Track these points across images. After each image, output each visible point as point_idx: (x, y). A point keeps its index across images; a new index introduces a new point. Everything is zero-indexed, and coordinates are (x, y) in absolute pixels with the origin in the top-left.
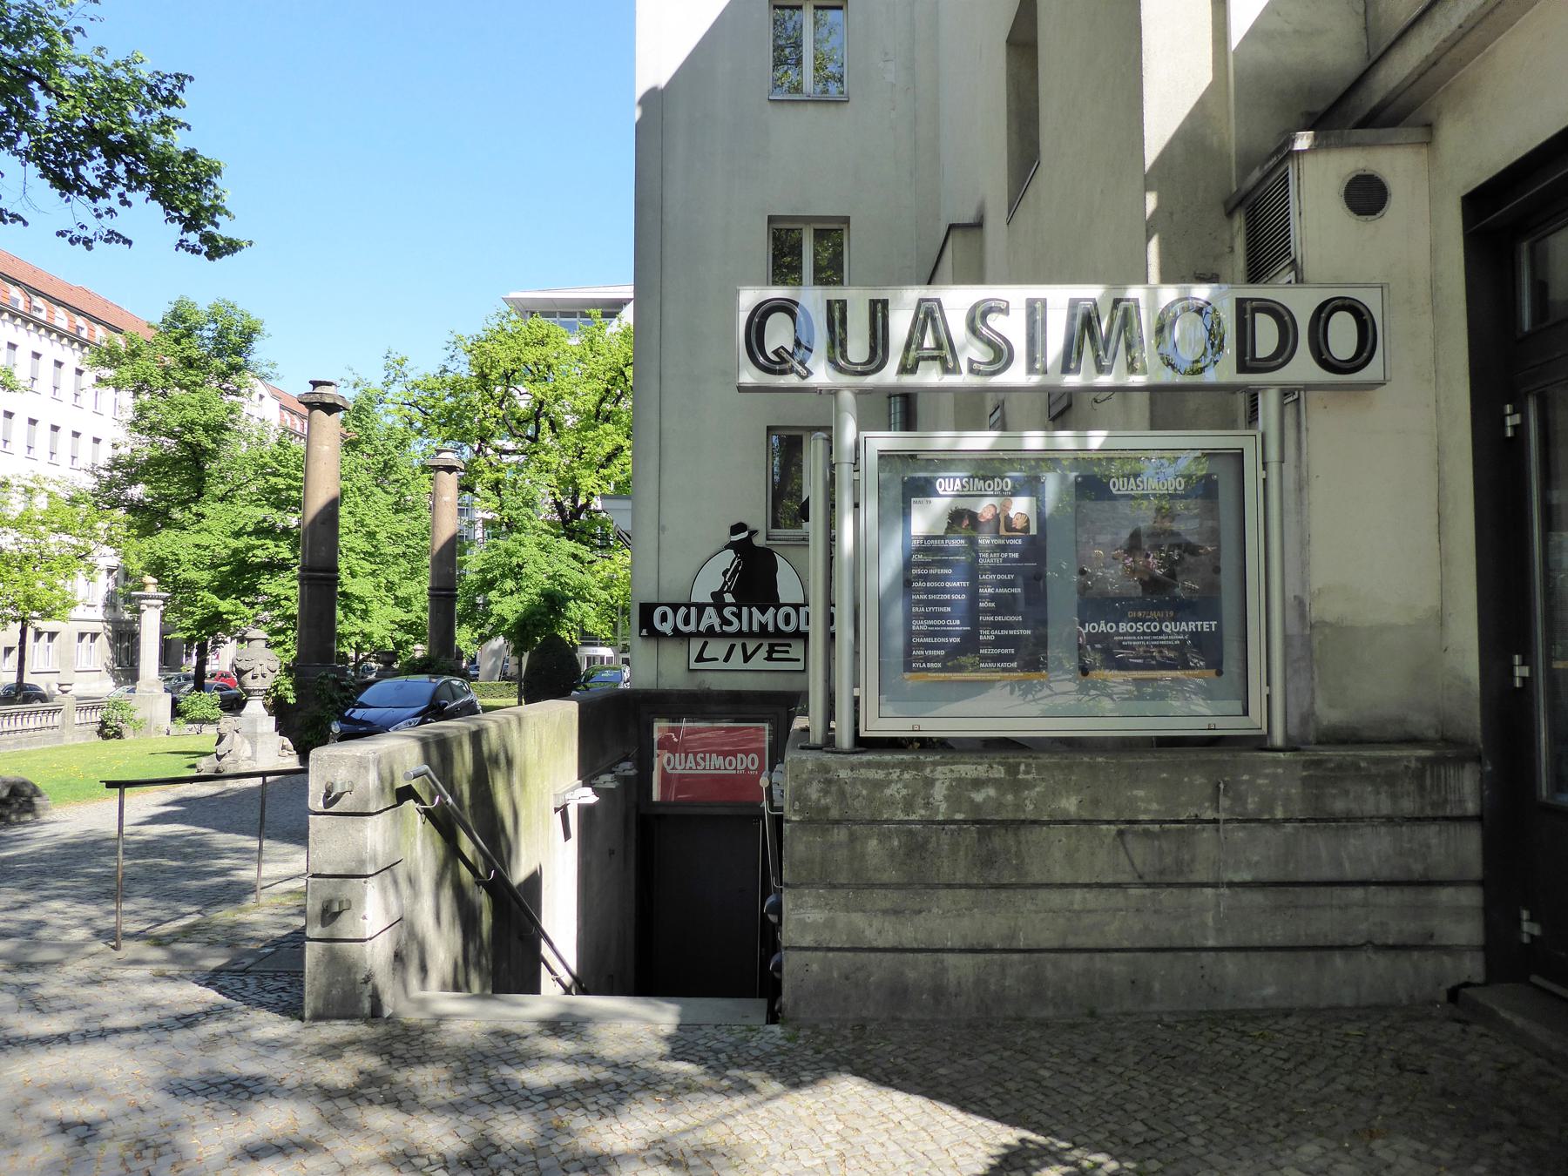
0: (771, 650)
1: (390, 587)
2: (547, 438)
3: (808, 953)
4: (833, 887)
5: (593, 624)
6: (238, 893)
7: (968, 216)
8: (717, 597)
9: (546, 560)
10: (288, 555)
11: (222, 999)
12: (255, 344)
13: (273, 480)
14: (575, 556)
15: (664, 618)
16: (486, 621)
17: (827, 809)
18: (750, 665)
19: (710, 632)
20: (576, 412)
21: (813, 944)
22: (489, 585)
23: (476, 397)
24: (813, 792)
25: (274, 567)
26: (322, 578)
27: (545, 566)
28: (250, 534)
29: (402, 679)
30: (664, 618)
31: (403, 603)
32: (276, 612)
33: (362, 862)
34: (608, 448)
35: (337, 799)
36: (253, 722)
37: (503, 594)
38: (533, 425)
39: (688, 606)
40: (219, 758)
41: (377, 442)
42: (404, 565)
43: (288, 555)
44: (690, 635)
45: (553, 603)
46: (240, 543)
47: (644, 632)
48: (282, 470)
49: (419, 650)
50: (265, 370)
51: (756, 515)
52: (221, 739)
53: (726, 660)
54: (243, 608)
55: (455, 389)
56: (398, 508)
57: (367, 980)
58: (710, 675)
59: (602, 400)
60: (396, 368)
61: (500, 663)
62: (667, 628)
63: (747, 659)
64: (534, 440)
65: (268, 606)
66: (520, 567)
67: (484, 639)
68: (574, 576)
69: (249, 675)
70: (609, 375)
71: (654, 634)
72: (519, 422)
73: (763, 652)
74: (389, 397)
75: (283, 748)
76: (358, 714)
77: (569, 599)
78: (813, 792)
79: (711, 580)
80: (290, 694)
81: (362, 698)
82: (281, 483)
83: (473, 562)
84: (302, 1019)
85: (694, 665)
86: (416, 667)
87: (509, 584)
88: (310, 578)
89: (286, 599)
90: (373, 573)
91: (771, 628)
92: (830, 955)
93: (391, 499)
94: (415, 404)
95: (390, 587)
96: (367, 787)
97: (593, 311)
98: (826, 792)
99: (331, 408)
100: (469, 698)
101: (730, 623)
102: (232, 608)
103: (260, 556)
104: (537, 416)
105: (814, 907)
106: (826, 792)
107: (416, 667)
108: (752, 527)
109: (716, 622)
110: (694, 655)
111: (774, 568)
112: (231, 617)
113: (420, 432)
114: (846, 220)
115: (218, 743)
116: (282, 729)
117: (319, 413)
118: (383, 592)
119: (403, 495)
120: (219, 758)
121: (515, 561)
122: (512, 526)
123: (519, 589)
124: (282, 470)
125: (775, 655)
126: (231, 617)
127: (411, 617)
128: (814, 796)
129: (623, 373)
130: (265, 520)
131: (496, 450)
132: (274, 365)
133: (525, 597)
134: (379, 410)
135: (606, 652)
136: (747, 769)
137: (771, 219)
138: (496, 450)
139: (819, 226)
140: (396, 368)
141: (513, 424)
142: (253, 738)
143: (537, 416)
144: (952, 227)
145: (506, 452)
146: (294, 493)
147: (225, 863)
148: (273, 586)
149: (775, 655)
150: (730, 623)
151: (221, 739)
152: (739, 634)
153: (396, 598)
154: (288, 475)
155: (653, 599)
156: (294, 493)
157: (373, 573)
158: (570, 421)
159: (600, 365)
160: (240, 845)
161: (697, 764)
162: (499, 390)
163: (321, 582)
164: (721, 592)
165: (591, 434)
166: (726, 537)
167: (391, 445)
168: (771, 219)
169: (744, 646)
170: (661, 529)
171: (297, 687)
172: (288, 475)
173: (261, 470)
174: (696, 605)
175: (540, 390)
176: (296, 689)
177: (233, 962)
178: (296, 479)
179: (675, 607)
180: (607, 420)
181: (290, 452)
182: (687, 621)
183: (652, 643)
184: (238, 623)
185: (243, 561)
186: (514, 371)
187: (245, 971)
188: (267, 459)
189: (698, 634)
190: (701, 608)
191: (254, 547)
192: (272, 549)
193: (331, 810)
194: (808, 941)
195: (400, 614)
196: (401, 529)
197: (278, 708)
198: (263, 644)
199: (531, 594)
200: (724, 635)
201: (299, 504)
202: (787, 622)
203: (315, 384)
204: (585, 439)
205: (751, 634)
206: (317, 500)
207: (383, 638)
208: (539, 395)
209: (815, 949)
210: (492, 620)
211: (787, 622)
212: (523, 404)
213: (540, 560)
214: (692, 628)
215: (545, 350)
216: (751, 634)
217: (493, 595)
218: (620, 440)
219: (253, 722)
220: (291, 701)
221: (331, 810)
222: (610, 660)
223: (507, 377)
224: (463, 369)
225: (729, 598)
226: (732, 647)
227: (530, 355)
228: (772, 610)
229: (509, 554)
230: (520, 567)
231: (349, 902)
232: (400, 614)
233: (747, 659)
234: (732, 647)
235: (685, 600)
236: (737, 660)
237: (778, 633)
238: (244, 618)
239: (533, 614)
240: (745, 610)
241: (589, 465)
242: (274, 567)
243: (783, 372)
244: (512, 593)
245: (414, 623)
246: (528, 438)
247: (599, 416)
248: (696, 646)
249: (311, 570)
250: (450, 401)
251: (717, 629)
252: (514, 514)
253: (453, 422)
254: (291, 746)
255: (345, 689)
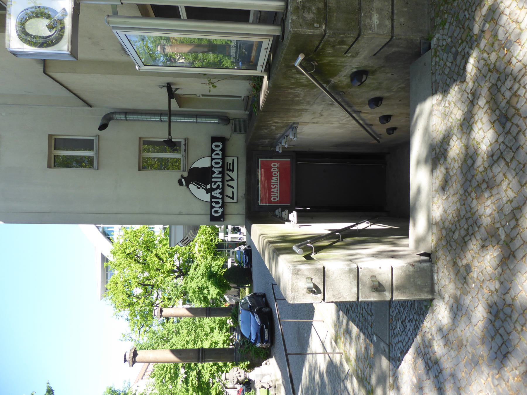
0: (229, 170)
1: (206, 335)
2: (153, 282)
3: (395, 23)
4: (360, 9)
5: (220, 262)
6: (333, 369)
7: (40, 68)
8: (208, 191)
9: (196, 279)
10: (195, 372)
11: (411, 351)
12: (116, 389)
13: (167, 379)
14: (195, 270)
15: (216, 212)
16: (219, 300)
17: (318, 9)
18: (235, 179)
19: (222, 193)
20: (143, 272)
21: (390, 21)
22: (205, 298)
23: (137, 308)
24: (309, 16)
25: (199, 375)
26: (202, 354)
27: (199, 279)
28: (187, 386)
29: (240, 323)
30: (216, 212)
31: (212, 330)
32: (216, 374)
33: (351, 270)
34: (156, 259)
35: (315, 286)
36: (257, 376)
37: (209, 293)
38: (148, 287)
39: (211, 202)
40: (270, 387)
41: (153, 342)
42: (198, 330)
43: (195, 372)
44: (223, 201)
45: (212, 276)
46: (191, 389)
47: (222, 219)
48: (163, 376)
49: (230, 322)
50: (126, 385)
51: (176, 175)
52: (263, 387)
53: (233, 188)
54: (214, 387)
55: (134, 315)
56: (178, 333)
57: (413, 266)
58: (239, 194)
59: (139, 262)
60: (125, 337)
61: (234, 297)
62: (220, 211)
63: (233, 180)
64: (153, 286)
65: (214, 378)
66: (199, 288)
67: (225, 301)
68: (202, 269)
69: (239, 378)
70: (129, 260)
71: (223, 215)
72: (147, 292)
73: (230, 173)
74: (137, 339)
75: (266, 364)
76: (253, 337)
77: (211, 270)
78: (309, 16)
79: (203, 195)
80: (246, 363)
81: (247, 336)
82: (168, 376)
83: (196, 304)
84: (432, 300)
85: (235, 200)
86: (235, 320)
87: (205, 291)
88: (202, 358)
89: (211, 371)
90: (202, 341)
91: (221, 170)
92: (395, 11)
93: (175, 336)
94: (140, 329)
95: (206, 335)
96: (309, 270)
97: (105, 266)
98: (309, 9)
99: (135, 354)
100: (247, 299)
101: (219, 186)
102: (214, 390)
103: (195, 382)
104: (144, 285)
105: (371, 18)
106: (309, 9)
107: (235, 320)
108: (180, 177)
109: (218, 191)
110: (231, 200)
111: (197, 169)
112: (218, 391)
113: (150, 327)
114: (50, 136)
115: (265, 388)
116: (259, 365)
117: (137, 359)
118: (209, 337)
119: (173, 332)
120: (270, 387)
121: (197, 290)
122: (185, 293)
123: (207, 287)
124: (163, 376)
125: (231, 169)
126: (218, 391)
127: (217, 327)
128: (312, 16)
129: (129, 254)
130: (182, 381)
131: (157, 299)
132: (125, 381)
133: (210, 286)
134: (141, 342)
135: (230, 261)
136: (277, 168)
137: (49, 167)
138: (157, 299)
139: (53, 148)
140: (125, 337)
141: (147, 293)
142: (263, 375)
143: (144, 285)
144: (45, 72)
145: (158, 296)
146: (172, 371)
147: (317, 378)
148: (206, 377)
149: (231, 169)
150: (219, 186)
151: (263, 387)
152: (223, 182)
153: (210, 333)
154: (165, 373)
155: (209, 217)
156: (172, 371)
157: (202, 341)
158: (146, 274)
159: (125, 262)
160: (307, 373)
161: (275, 187)
162: (135, 300)
163: (202, 355)
164: (206, 190)
165: (151, 265)
166: (184, 188)
167: (154, 337)
168: (49, 167)
169: (228, 181)
170: (180, 214)
171: (243, 361)
172: (165, 373)
173: (163, 384)
174: (211, 199)
175: (134, 283)
176: (245, 361)
177: (384, 353)
178: (167, 371)
179: (212, 207)
180: (146, 260)
181: (157, 373)
182: (218, 203)
183: (227, 217)
184: (220, 388)
185: (197, 387)
186: (127, 294)
187: (389, 345)
188: (159, 381)
189: (223, 198)
190: (212, 197)
191: (192, 384)
192: (193, 377)
193: (322, 289)
194: (388, 23)
195: (216, 331)
196: (185, 331)
197: (251, 367)
198: (227, 374)
199: (209, 284)
200: (223, 188)
201: (176, 368)
202: (218, 163)
203: (125, 361)
204: (153, 267)
205: (223, 177)
206: (172, 357)
207: (225, 336)
208: (136, 284)
209: (393, 20)
210: (218, 298)
211: (218, 163)
212: (139, 291)
213: (197, 281)
214: (220, 201)
215: (119, 283)
216: (223, 177)
217: (209, 297)
218: (153, 255)
219: (257, 376)
220: (249, 362)
221: (322, 289)
222: (232, 260)
223: (129, 296)
224: (127, 312)
225: (208, 187)
226: (228, 185)
227: (121, 287)
228: (213, 169)
229: (194, 292)
230: (199, 288)
231: (372, 276)
232: (216, 331)
233: (233, 180)
234: (228, 185)
235: (209, 204)
236: (234, 184)
237: (222, 167)
238: (218, 385)
239: (216, 283)
240: (213, 180)
241: (162, 266)
242: (199, 375)
243: (63, 28)
244: (209, 291)
245: (219, 327)
246: (152, 288)
247: (145, 264)
248: (228, 200)
249: (199, 359)
250: (138, 317)
251: (221, 191)
252: (179, 291)
253: (147, 316)
254: (266, 361)
255: (244, 343)
